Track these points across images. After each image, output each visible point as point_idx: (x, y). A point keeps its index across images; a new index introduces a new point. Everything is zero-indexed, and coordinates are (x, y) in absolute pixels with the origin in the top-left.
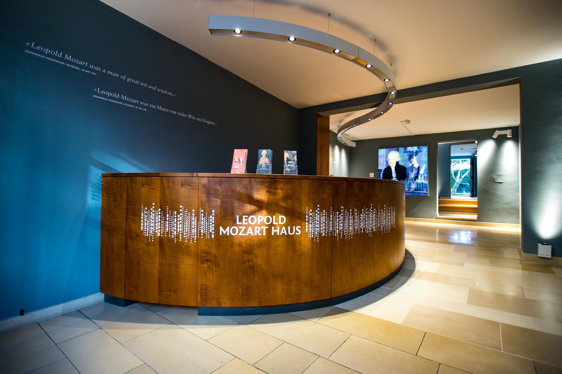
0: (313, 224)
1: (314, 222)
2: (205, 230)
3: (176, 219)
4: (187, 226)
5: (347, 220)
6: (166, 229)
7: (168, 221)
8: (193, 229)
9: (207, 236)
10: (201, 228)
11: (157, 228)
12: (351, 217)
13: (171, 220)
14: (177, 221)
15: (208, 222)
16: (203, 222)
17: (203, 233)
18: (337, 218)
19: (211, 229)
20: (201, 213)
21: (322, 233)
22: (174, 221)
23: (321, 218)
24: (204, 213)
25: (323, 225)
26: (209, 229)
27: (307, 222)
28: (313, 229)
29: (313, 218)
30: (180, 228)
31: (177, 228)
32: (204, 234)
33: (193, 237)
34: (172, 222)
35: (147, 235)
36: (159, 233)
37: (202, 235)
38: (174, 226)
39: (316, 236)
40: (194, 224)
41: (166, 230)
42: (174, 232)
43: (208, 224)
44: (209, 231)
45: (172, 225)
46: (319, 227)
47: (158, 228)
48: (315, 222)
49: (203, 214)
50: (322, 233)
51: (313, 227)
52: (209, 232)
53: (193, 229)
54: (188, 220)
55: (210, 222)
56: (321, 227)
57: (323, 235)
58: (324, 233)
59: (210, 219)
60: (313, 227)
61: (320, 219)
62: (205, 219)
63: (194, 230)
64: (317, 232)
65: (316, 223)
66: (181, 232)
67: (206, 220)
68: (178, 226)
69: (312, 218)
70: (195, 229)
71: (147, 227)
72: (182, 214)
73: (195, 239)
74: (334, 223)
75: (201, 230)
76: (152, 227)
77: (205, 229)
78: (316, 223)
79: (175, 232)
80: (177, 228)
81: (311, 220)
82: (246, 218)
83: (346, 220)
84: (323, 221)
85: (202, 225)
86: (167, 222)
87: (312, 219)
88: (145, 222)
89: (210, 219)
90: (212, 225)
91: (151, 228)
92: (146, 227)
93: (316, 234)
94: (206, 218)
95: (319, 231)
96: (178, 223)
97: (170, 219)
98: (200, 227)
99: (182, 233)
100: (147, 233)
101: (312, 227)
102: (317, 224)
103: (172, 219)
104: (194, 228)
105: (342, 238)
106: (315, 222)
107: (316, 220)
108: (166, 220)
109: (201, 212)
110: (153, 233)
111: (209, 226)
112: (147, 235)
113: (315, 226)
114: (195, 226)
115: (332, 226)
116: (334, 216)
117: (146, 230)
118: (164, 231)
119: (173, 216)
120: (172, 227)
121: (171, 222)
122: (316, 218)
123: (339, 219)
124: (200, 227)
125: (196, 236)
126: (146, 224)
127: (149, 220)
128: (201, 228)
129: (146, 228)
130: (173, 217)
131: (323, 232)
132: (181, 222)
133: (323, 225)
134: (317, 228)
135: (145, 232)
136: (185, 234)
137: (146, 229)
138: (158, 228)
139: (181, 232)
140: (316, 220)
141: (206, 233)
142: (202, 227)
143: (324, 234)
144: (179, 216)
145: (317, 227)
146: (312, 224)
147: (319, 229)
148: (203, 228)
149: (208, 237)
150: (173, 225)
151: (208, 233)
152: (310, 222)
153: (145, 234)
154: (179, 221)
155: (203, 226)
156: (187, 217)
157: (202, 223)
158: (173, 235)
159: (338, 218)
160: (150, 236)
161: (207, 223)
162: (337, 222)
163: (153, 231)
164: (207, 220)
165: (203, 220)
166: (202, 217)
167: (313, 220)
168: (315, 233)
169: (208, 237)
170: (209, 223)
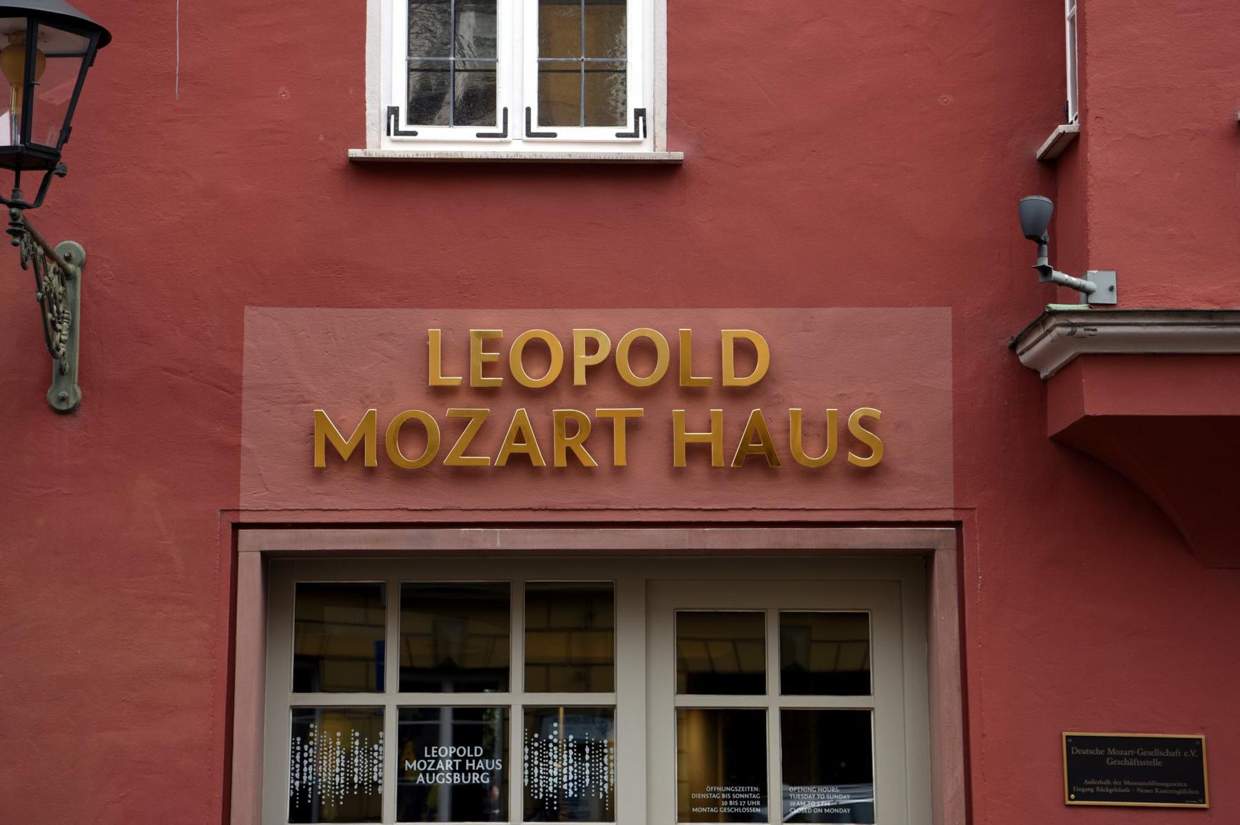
0: (543, 767)
1: (543, 763)
2: (363, 778)
3: (606, 756)
4: (325, 769)
5: (328, 758)
6: (584, 780)
7: (590, 761)
8: (337, 776)
9: (368, 790)
10: (354, 773)
11: (565, 779)
12: (338, 753)
13: (595, 758)
14: (302, 758)
15: (369, 759)
16: (359, 758)
17: (358, 783)
18: (298, 751)
19: (375, 773)
20: (354, 741)
21: (566, 789)
22: (603, 762)
23: (563, 754)
24: (361, 739)
25: (568, 771)
26: (373, 775)
27: (588, 761)
28: (543, 780)
29: (542, 753)
30: (308, 775)
31: (302, 775)
32: (361, 786)
33: (337, 793)
34: (598, 763)
35: (541, 795)
36: (570, 790)
37: (356, 787)
38: (604, 771)
39: (551, 796)
40: (340, 763)
41: (584, 782)
42: (602, 786)
43: (368, 764)
44: (372, 779)
45: (600, 769)
46: (558, 776)
47: (568, 778)
48: (546, 763)
49: (358, 740)
50: (566, 789)
51: (543, 775)
52: (370, 781)
53: (337, 776)
54: (327, 756)
55: (374, 758)
56: (563, 775)
57: (568, 795)
58: (570, 790)
59: (374, 751)
60: (543, 775)
61: (559, 756)
62: (363, 751)
63: (340, 777)
64: (553, 786)
65: (549, 765)
66: (310, 784)
67: (365, 753)
68: (305, 769)
69: (540, 753)
70: (342, 774)
71: (539, 779)
72: (533, 746)
73: (341, 797)
74: (595, 767)
75: (354, 777)
76: (554, 777)
77: (363, 773)
78: (549, 765)
79: (606, 786)
80: (302, 775)
81: (536, 758)
82: (435, 750)
83: (325, 757)
84: (568, 762)
85: (356, 765)
86: (587, 765)
87: (538, 756)
88: (533, 767)
89: (374, 751)
90: (378, 764)
91: (551, 779)
92: (538, 777)
93: (551, 791)
94: (365, 749)
95: (558, 785)
96: (305, 762)
97: (593, 756)
98: (351, 771)
99: (312, 786)
100: (539, 791)
101: (539, 774)
102: (553, 769)
103: (597, 756)
104: (339, 774)
105: (356, 793)
106: (546, 763)
107: (549, 759)
108: (584, 761)
109: (354, 736)
110: (555, 791)
111: (373, 767)
112: (541, 795)
113: (548, 771)
114: (343, 769)
115: (591, 773)
116: (595, 750)
117: (536, 786)
118: (580, 785)
119: (601, 750)
120: (600, 774)
121: (595, 763)
122: (551, 754)
123: (302, 756)
124: (351, 771)
125: (343, 790)
126: (536, 771)
127: (544, 761)
128: (354, 773)
129: (536, 780)
130: (600, 752)
131: (568, 787)
132: (311, 760)
133: (568, 771)
134: (554, 777)
135: (534, 789)
136: (319, 787)
137: (538, 783)
138: (568, 778)
139: (310, 784)
140: (549, 759)
141: (366, 784)
142: (356, 770)
143: (571, 793)
144: (306, 747)
145: (551, 775)
146: (538, 766)
147: (559, 781)
148: (359, 771)
149: (369, 792)
150: (601, 771)
151: (369, 784)
152: (533, 763)
153: (535, 794)
154: (307, 758)
155: (359, 767)
156: (326, 749)
157: (356, 760)
158: (601, 793)
159: (299, 753)
160: (548, 797)
161: (367, 761)
162: (604, 765)
163: (555, 786)
164: (368, 753)
165: (359, 754)
166: (357, 748)
167: (542, 757)
168: (548, 788)
169: (369, 792)
170: (371, 761)
